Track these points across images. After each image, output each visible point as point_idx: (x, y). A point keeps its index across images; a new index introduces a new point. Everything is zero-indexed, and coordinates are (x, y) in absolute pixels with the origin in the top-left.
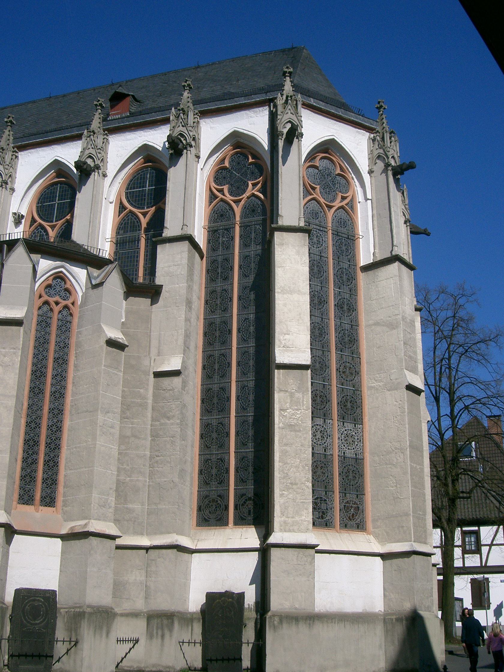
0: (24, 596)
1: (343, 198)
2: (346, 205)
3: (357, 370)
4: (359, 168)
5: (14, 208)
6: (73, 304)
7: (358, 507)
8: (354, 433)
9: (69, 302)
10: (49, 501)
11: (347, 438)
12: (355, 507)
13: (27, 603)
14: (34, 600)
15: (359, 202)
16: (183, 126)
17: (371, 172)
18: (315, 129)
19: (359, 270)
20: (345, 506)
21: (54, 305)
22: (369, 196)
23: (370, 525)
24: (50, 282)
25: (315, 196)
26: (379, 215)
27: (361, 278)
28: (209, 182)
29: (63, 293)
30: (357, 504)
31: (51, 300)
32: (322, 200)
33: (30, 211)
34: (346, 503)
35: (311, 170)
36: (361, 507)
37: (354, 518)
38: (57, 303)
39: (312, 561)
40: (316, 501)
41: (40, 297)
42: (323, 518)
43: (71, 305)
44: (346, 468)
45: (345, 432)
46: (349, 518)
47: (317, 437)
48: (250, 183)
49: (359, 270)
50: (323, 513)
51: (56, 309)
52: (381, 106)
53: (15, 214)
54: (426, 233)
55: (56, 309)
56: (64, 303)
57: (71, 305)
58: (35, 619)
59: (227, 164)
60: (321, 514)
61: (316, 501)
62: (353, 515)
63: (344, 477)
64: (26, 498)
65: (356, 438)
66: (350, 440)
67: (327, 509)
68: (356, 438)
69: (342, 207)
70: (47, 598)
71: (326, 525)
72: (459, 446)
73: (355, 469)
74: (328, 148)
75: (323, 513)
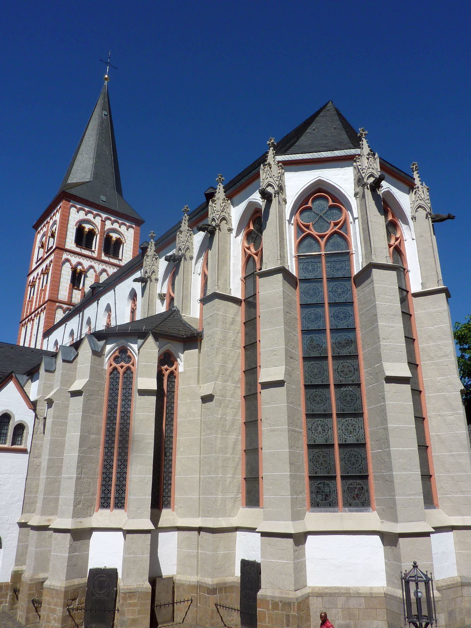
0: (96, 573)
1: (336, 224)
2: (340, 228)
3: (355, 367)
4: (346, 194)
5: (158, 291)
6: (133, 365)
7: (363, 488)
8: (354, 423)
9: (129, 365)
10: (120, 504)
11: (347, 427)
12: (359, 489)
13: (97, 579)
14: (101, 577)
15: (351, 223)
16: (420, 200)
17: (356, 195)
18: (296, 183)
19: (259, 386)
20: (348, 488)
21: (124, 368)
22: (356, 215)
23: (374, 503)
24: (117, 354)
25: (308, 231)
26: (363, 229)
27: (404, 229)
28: (243, 244)
29: (127, 359)
30: (361, 485)
31: (118, 366)
32: (314, 233)
33: (168, 289)
34: (349, 485)
35: (306, 214)
36: (365, 487)
37: (359, 498)
38: (122, 367)
39: (265, 600)
40: (320, 486)
41: (111, 365)
42: (326, 500)
43: (131, 366)
44: (348, 453)
45: (346, 423)
46: (354, 498)
47: (318, 431)
48: (332, 222)
49: (259, 386)
50: (327, 495)
51: (121, 371)
52: (362, 134)
53: (159, 294)
54: (450, 217)
55: (121, 371)
56: (126, 365)
57: (131, 366)
58: (101, 590)
59: (252, 227)
60: (324, 496)
61: (320, 486)
62: (357, 495)
63: (346, 462)
64: (105, 504)
65: (357, 426)
66: (350, 428)
67: (330, 492)
68: (357, 426)
69: (335, 232)
70: (112, 574)
71: (330, 505)
72: (78, 271)
73: (357, 453)
74: (319, 192)
75: (327, 495)
